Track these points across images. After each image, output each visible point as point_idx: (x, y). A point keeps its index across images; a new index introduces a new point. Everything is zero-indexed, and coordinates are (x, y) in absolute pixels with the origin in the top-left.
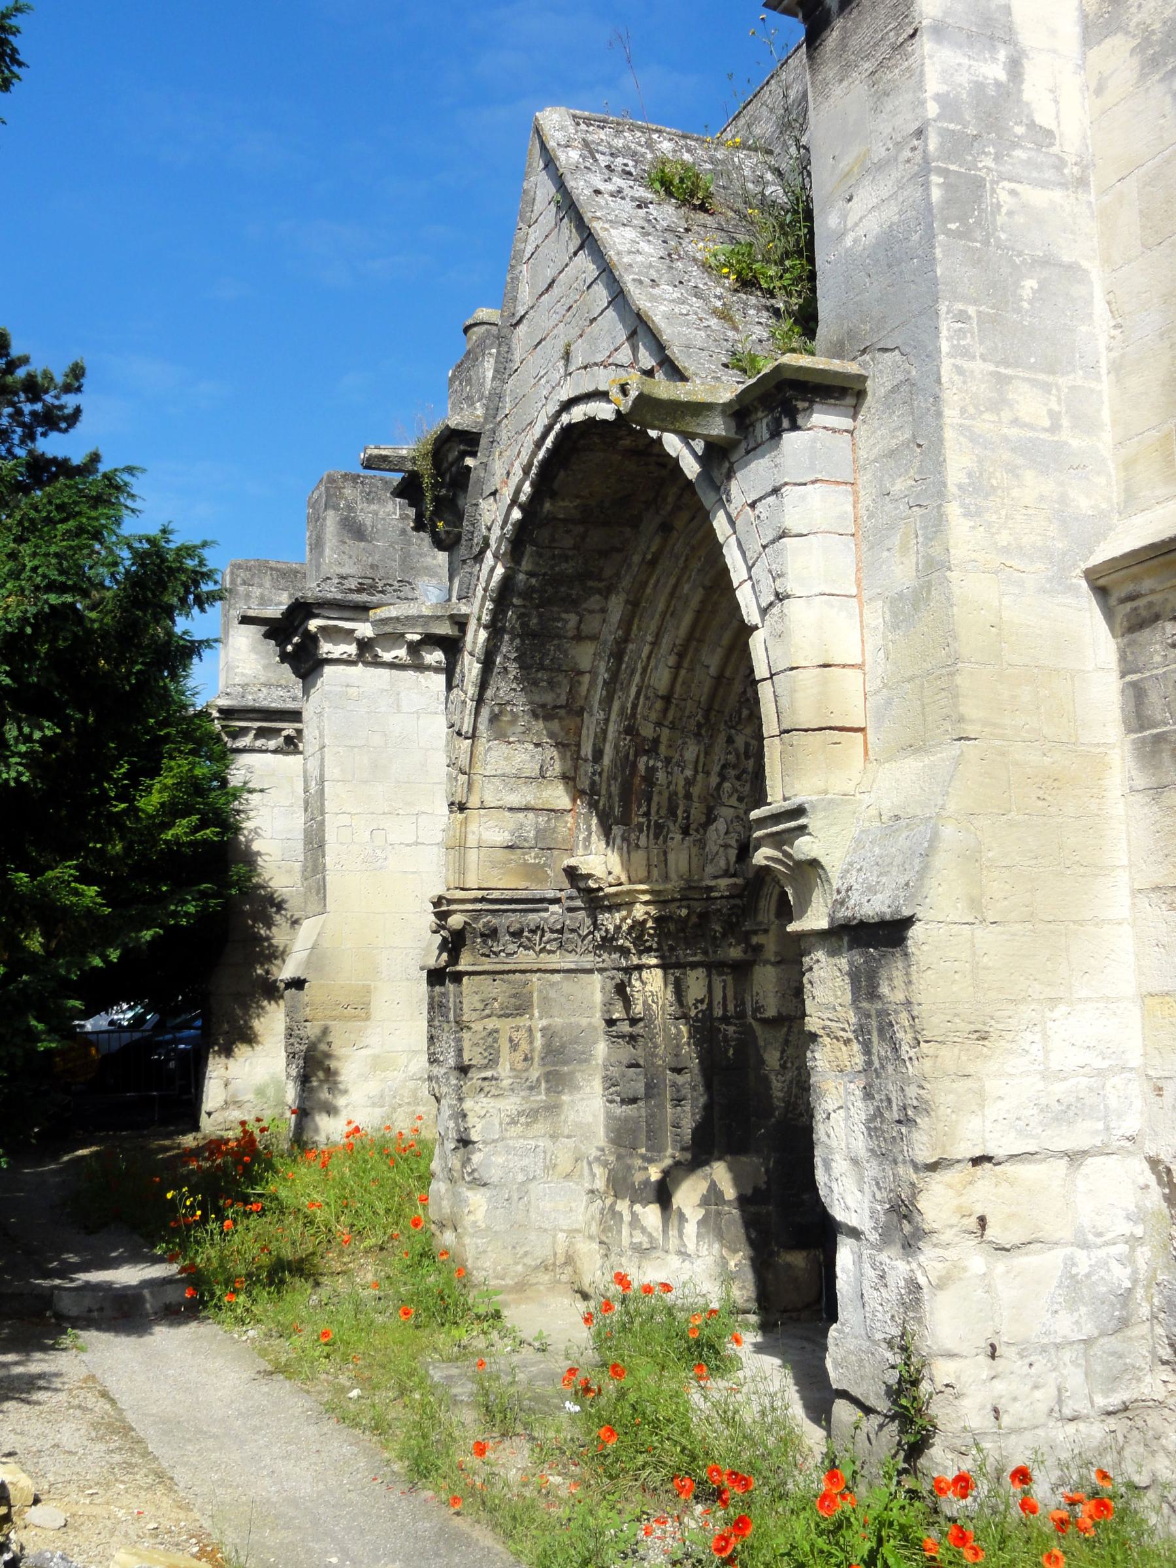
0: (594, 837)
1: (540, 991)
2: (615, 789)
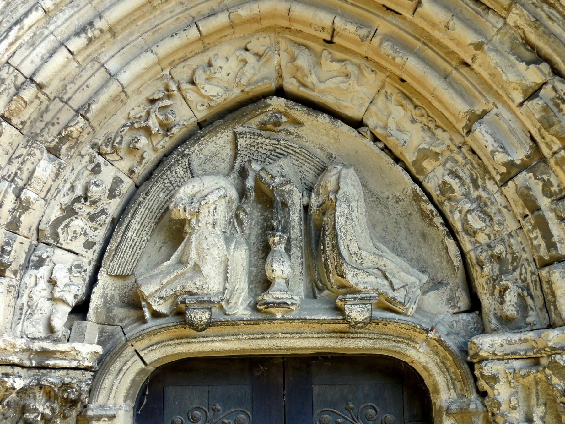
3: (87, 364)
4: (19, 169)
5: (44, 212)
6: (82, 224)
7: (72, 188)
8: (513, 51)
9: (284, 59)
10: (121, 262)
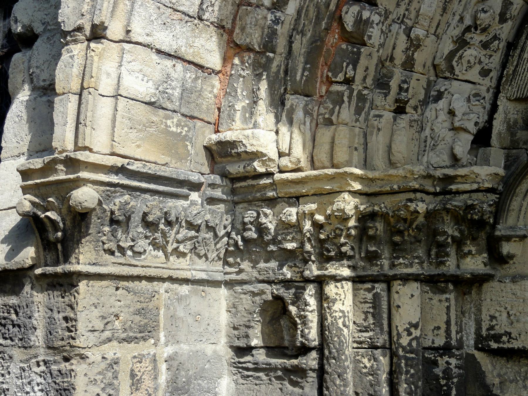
0: (262, 106)
1: (167, 308)
2: (300, 46)
3: (487, 185)
4: (407, 10)
5: (438, 48)
6: (474, 53)
7: (461, 20)
10: (519, 85)
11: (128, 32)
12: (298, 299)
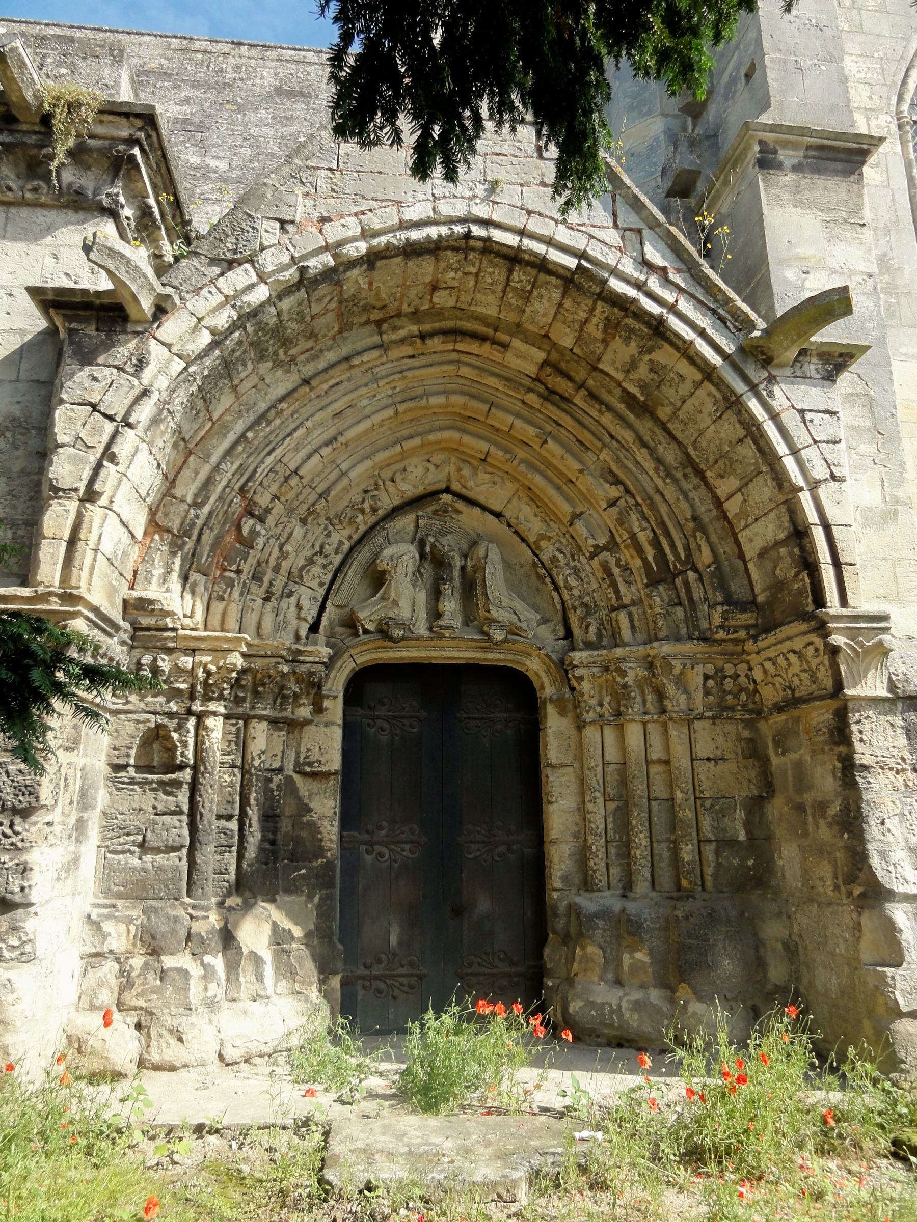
7: (313, 546)
8: (602, 476)
9: (453, 469)
11: (112, 502)
12: (180, 728)
